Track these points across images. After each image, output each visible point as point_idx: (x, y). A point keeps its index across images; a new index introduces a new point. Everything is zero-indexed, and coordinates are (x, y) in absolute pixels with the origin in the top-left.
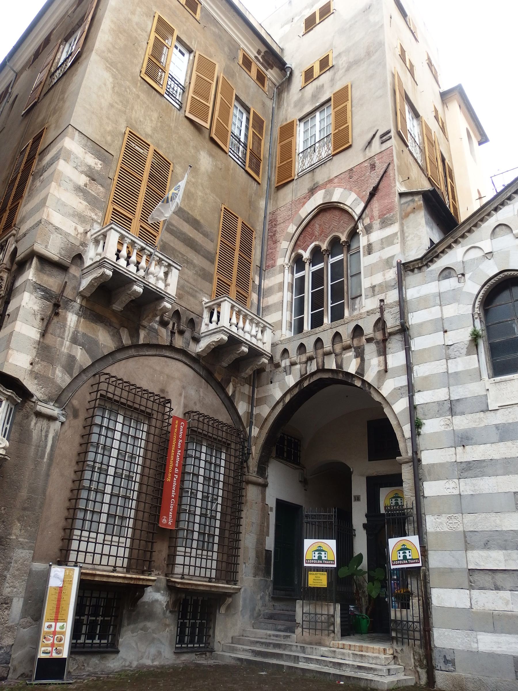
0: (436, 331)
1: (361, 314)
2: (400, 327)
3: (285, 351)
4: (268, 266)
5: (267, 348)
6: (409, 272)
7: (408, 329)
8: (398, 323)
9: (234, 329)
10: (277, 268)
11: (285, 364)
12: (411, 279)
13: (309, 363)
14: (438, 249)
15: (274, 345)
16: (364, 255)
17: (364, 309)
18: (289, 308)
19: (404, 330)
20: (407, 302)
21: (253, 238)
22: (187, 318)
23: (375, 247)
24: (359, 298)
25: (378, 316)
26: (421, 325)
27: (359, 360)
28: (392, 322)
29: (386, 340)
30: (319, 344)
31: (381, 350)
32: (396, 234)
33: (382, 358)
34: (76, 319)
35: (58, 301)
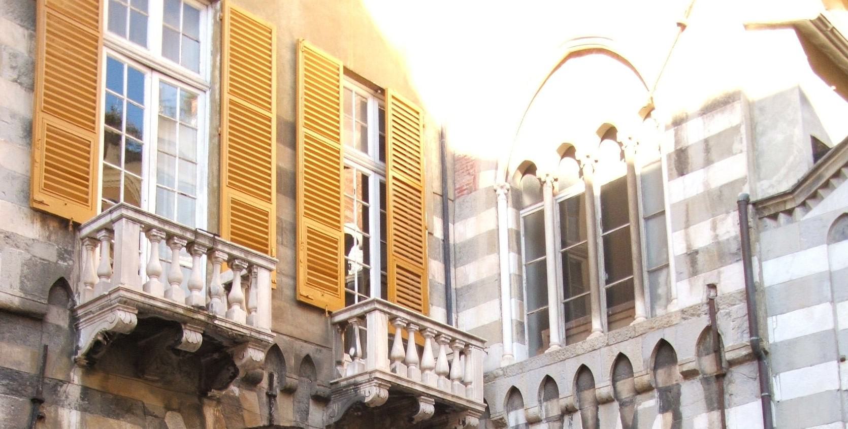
0: (824, 359)
1: (669, 316)
2: (750, 351)
3: (514, 392)
4: (461, 190)
5: (475, 395)
6: (768, 222)
7: (766, 353)
8: (746, 339)
9: (401, 371)
10: (480, 195)
11: (517, 420)
12: (772, 235)
13: (566, 419)
14: (827, 169)
15: (489, 378)
16: (671, 178)
17: (677, 302)
18: (515, 291)
19: (758, 354)
20: (763, 291)
21: (421, 128)
22: (297, 356)
23: (696, 156)
24: (664, 272)
25: (705, 321)
26: (791, 344)
27: (669, 416)
28: (734, 340)
29: (724, 375)
30: (584, 378)
31: (715, 397)
32: (736, 129)
33: (716, 414)
34: (79, 418)
35: (38, 392)
